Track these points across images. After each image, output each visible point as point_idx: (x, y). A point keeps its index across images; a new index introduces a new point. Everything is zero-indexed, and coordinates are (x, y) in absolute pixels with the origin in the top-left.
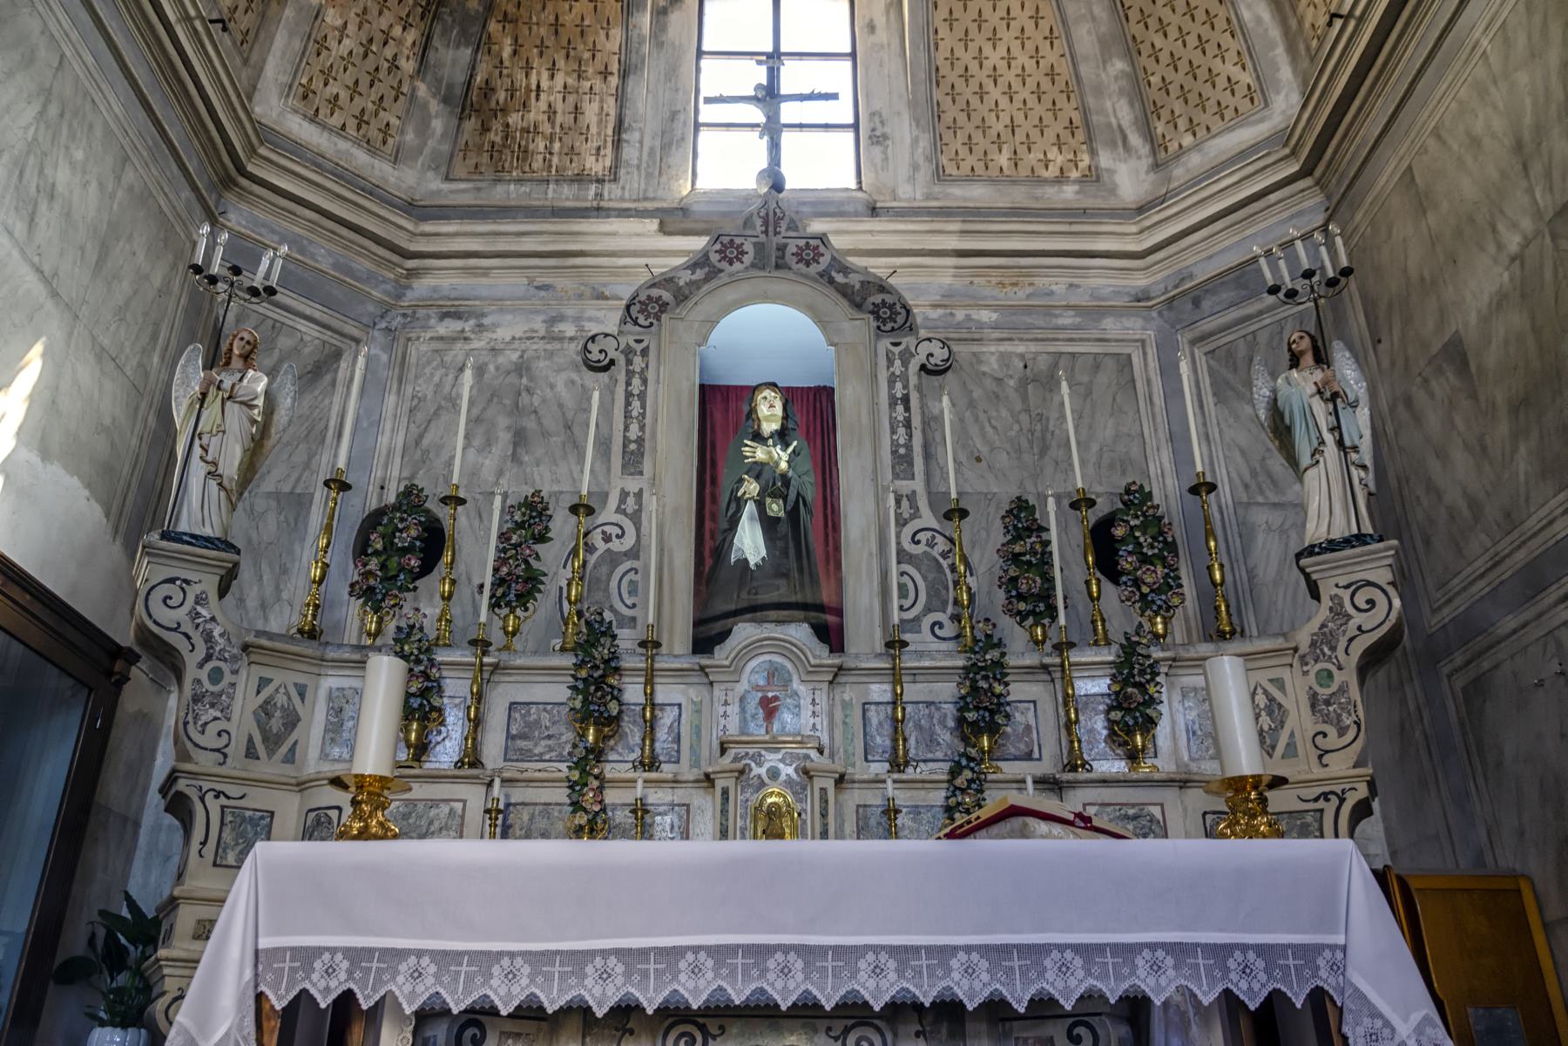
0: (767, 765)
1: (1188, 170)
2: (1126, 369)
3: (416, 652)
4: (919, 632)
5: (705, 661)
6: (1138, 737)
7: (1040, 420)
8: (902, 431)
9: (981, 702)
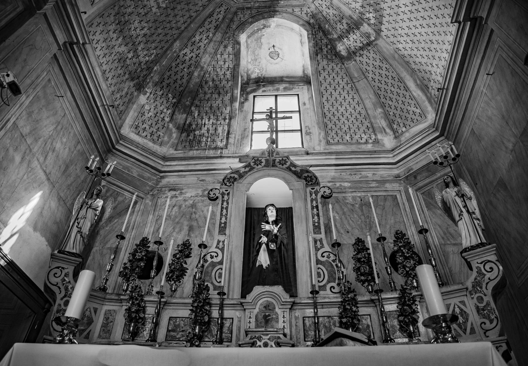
0: (263, 341)
1: (406, 138)
2: (395, 200)
3: (137, 296)
4: (326, 290)
5: (243, 301)
6: (411, 327)
7: (368, 218)
8: (316, 217)
9: (347, 314)
